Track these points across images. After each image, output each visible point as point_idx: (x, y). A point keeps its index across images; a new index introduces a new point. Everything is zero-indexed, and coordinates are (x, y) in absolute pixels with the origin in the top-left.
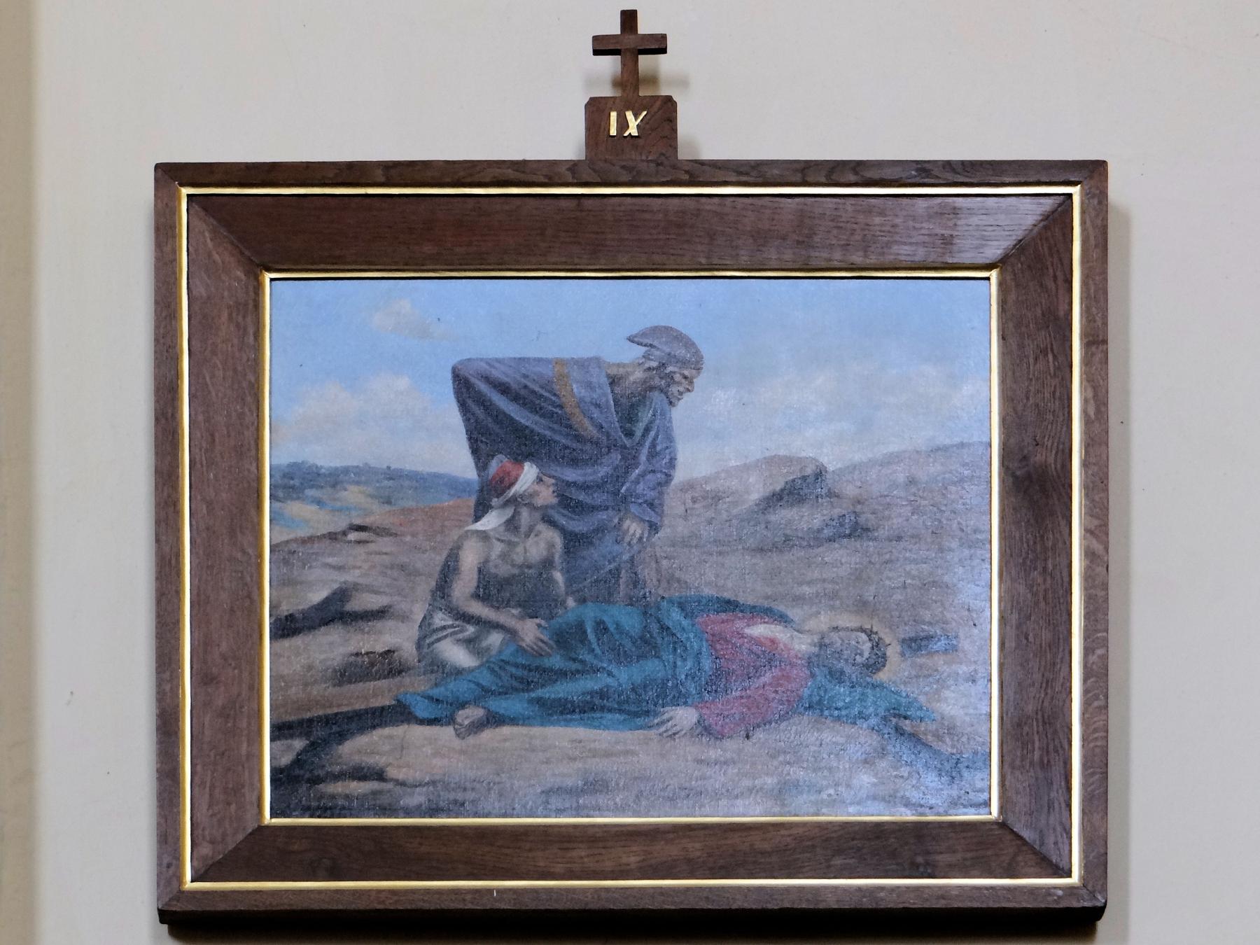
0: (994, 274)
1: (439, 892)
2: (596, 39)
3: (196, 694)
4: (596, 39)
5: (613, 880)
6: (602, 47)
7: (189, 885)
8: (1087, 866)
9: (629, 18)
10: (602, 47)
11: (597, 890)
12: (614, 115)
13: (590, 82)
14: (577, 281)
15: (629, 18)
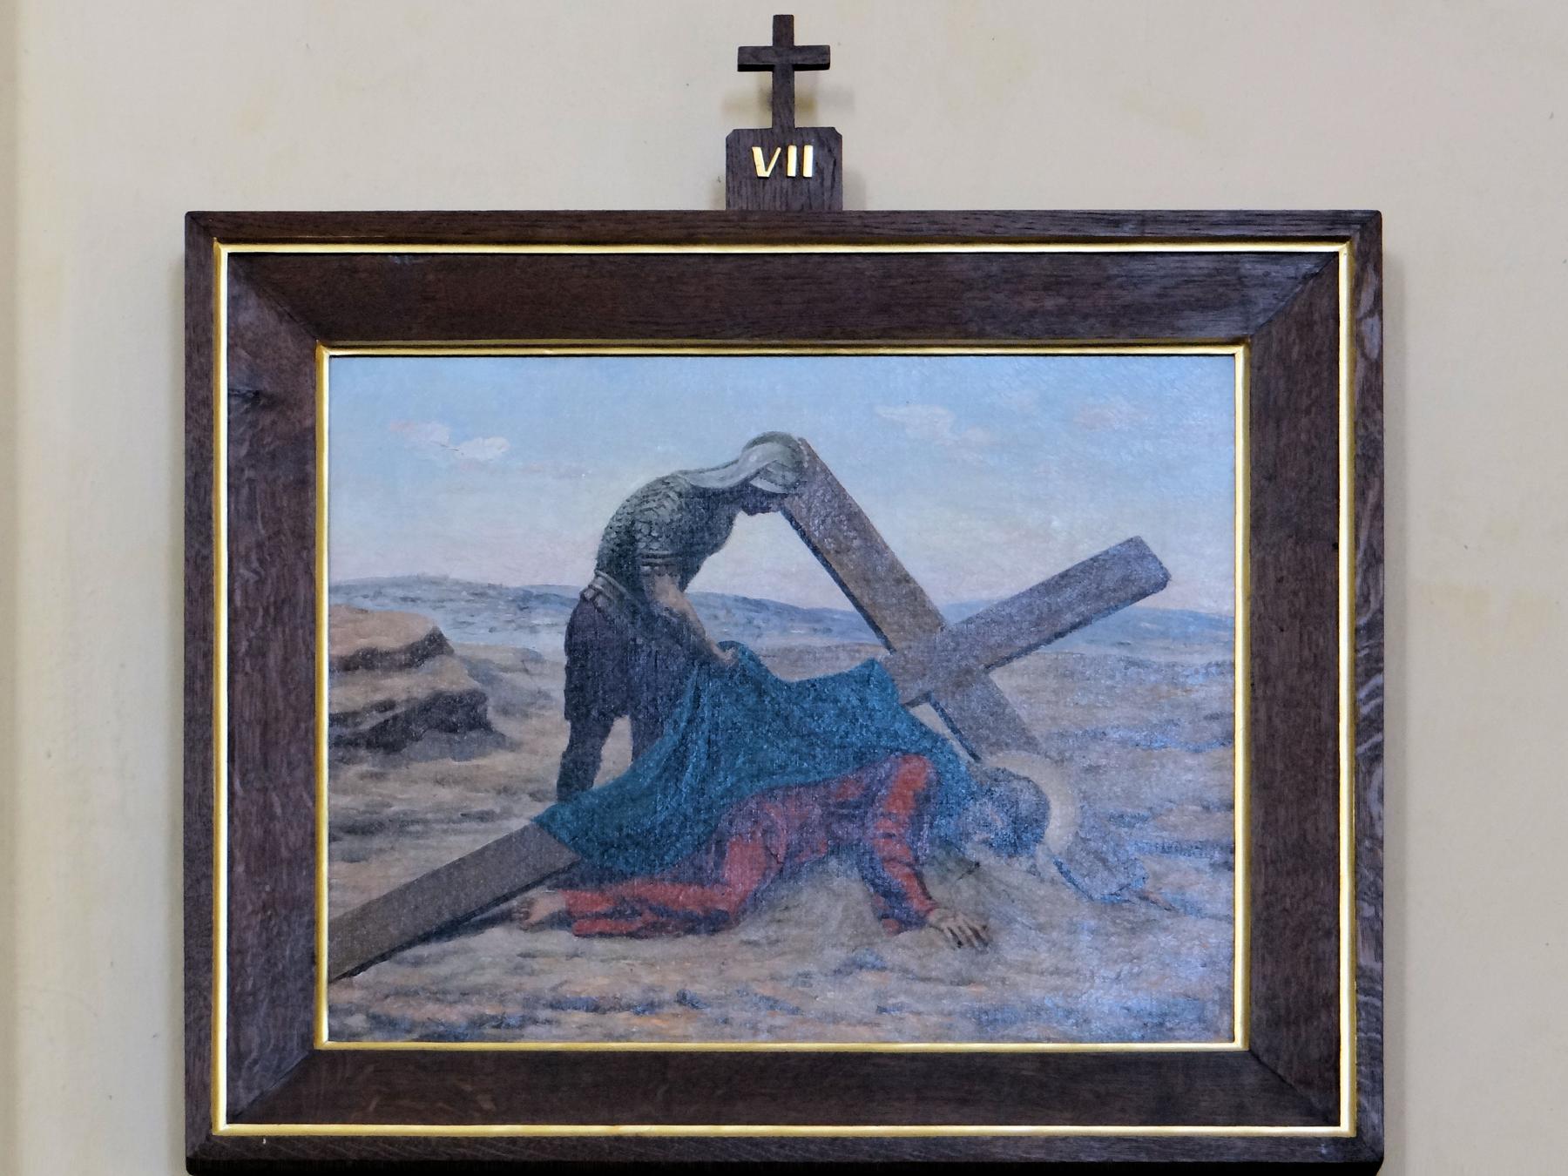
0: (1239, 351)
1: (953, 1140)
2: (742, 50)
3: (1270, 891)
4: (742, 50)
5: (1204, 1125)
6: (749, 61)
7: (222, 1126)
8: (1360, 1111)
9: (783, 25)
10: (749, 61)
11: (926, 1141)
12: (808, 171)
13: (731, 106)
14: (665, 358)
15: (783, 25)
